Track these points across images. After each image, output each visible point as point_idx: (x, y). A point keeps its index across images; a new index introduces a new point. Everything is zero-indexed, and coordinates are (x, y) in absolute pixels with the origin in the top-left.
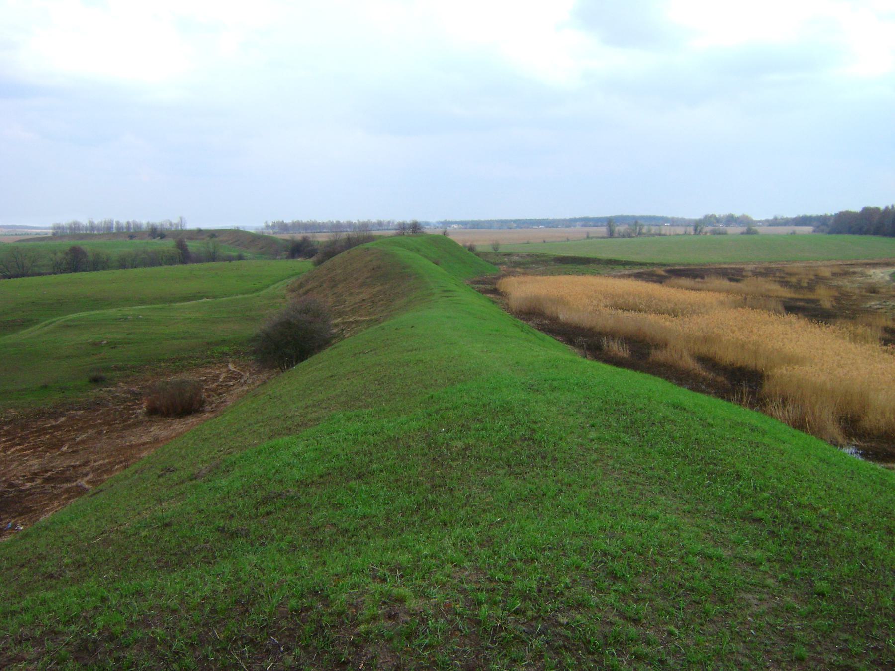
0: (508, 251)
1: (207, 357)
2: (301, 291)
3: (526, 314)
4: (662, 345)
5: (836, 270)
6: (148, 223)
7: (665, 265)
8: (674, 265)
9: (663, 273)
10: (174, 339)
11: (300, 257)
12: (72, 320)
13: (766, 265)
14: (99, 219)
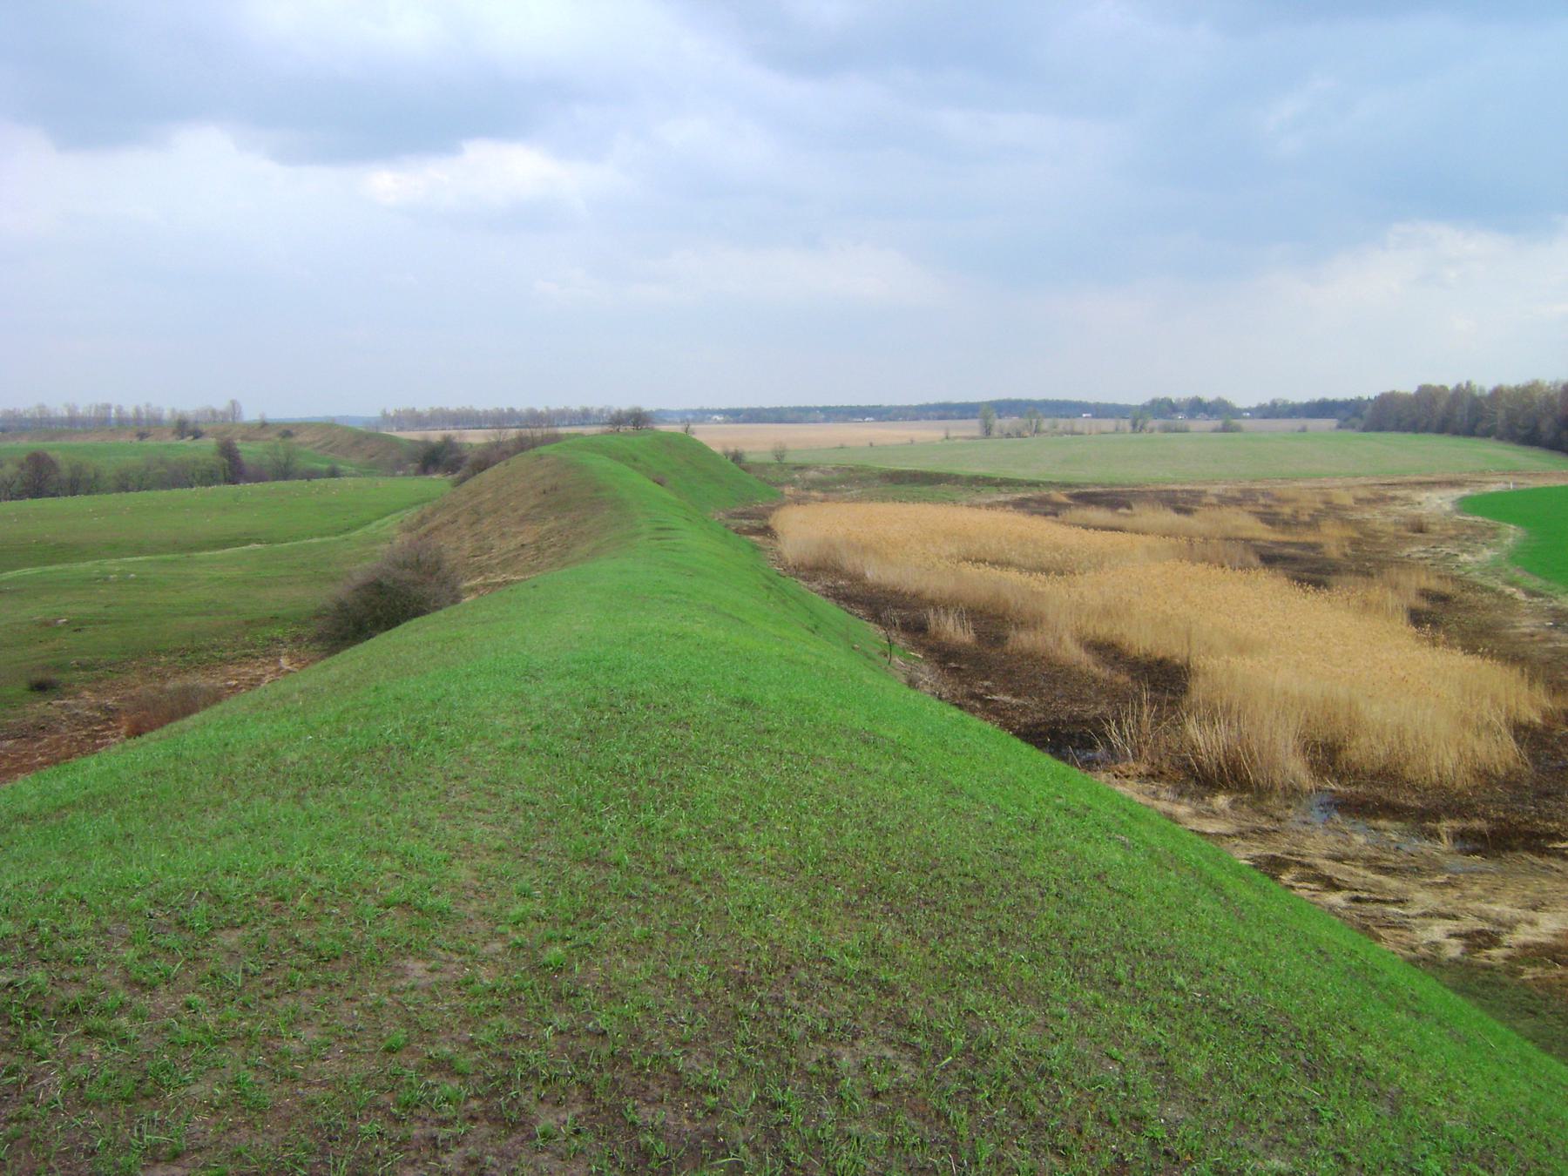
0: (798, 461)
1: (245, 646)
2: (422, 530)
3: (811, 569)
4: (1034, 622)
5: (1362, 493)
6: (173, 411)
7: (1068, 485)
8: (1086, 485)
9: (1065, 500)
10: (188, 614)
11: (436, 471)
12: (9, 582)
13: (1246, 485)
14: (395, 403)
